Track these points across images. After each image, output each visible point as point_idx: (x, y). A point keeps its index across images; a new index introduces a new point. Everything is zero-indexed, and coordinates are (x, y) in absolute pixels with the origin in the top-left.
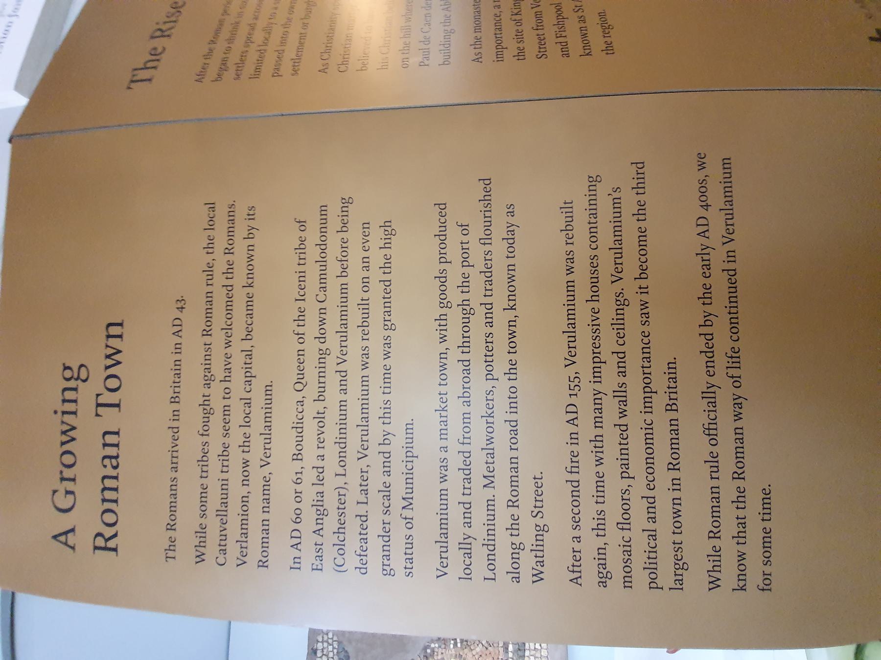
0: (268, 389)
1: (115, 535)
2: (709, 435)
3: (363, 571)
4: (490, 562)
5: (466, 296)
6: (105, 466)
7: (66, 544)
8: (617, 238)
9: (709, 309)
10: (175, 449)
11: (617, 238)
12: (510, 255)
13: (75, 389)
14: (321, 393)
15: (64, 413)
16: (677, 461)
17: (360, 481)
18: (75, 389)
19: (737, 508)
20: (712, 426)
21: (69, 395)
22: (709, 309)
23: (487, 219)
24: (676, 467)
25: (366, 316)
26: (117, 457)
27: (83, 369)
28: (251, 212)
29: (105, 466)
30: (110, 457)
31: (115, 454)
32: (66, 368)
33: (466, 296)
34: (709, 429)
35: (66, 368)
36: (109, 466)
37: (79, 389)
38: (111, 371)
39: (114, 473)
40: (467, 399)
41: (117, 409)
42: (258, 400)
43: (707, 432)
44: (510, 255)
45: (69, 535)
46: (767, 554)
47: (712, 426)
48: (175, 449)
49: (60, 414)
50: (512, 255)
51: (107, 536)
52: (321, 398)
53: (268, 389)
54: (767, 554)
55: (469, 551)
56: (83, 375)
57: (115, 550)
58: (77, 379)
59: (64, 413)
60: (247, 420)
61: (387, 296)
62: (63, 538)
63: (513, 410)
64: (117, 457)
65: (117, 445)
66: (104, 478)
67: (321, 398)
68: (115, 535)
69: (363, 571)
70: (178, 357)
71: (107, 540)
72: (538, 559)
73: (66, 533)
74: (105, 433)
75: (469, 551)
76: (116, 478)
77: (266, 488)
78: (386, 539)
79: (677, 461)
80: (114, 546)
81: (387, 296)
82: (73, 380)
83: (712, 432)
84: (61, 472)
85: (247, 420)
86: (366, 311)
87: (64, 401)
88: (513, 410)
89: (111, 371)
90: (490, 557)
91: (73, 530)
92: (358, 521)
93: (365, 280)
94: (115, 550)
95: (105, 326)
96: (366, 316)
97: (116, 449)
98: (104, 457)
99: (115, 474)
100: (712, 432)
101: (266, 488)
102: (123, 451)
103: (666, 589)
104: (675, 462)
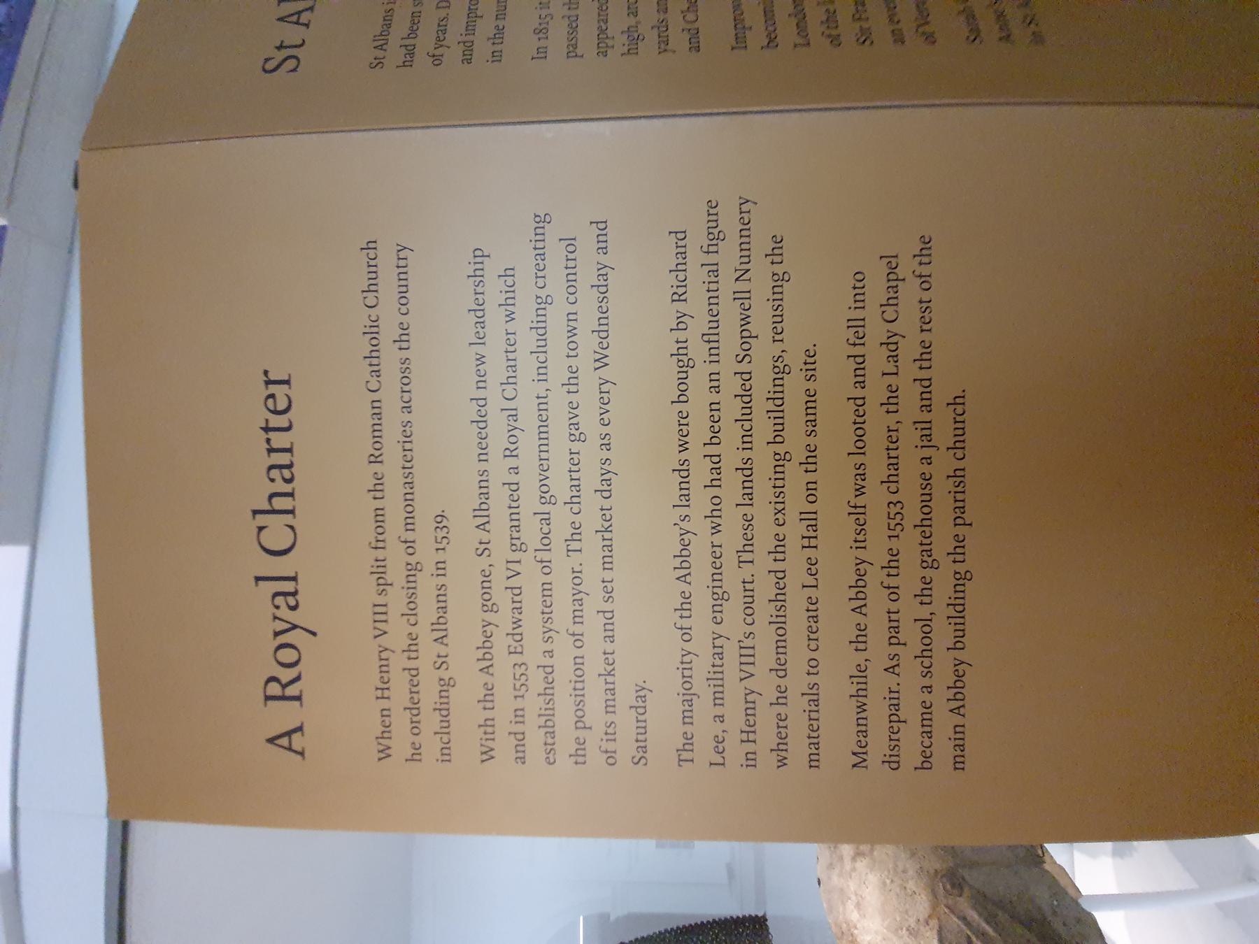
1: (298, 678)
3: (606, 494)
6: (272, 480)
7: (290, 749)
19: (921, 368)
25: (780, 427)
26: (290, 466)
28: (860, 538)
29: (272, 480)
30: (281, 467)
31: (292, 590)
38: (283, 639)
39: (287, 488)
41: (297, 703)
51: (284, 681)
57: (298, 698)
60: (546, 541)
61: (859, 420)
62: (284, 741)
64: (290, 466)
68: (298, 678)
69: (606, 494)
70: (441, 580)
71: (284, 686)
73: (289, 734)
76: (291, 495)
80: (296, 693)
81: (859, 420)
84: (268, 441)
85: (546, 541)
86: (780, 421)
89: (283, 639)
91: (300, 729)
94: (298, 698)
95: (265, 471)
96: (780, 427)
97: (293, 583)
98: (271, 467)
99: (290, 491)
103: (943, 449)
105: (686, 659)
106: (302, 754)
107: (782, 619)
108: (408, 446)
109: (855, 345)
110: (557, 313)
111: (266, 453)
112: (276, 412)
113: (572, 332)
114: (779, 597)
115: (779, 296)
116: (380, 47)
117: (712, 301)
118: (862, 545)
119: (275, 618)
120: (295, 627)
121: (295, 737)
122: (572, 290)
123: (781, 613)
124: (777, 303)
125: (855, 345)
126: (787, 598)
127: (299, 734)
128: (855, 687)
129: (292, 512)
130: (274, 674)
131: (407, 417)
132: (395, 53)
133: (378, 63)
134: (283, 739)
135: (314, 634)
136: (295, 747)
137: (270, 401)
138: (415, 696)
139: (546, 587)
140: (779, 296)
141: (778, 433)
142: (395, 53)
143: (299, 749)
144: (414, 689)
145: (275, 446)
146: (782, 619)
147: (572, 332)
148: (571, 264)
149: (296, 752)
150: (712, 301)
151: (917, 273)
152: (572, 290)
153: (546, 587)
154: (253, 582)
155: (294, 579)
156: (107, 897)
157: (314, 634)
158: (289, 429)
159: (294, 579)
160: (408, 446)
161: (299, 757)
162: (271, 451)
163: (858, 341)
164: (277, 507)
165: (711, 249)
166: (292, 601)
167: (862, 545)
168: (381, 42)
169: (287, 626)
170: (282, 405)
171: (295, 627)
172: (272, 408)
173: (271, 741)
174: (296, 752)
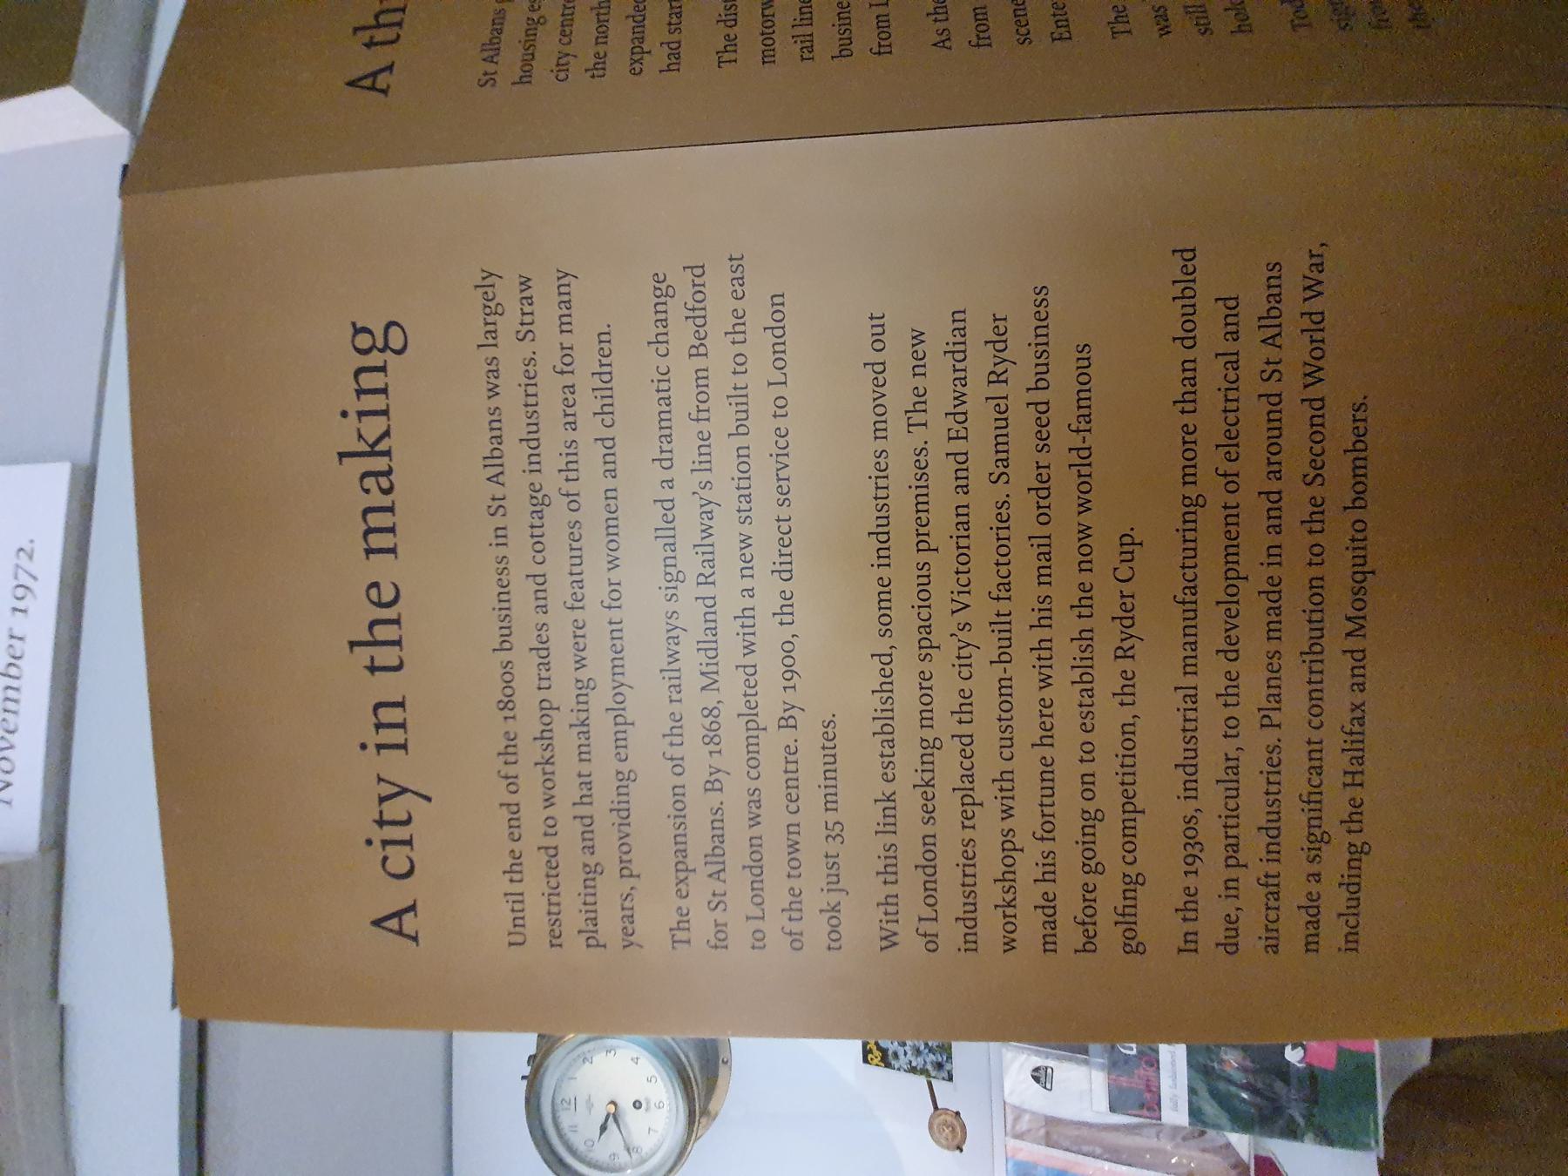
0: (604, 337)
5: (892, 890)
6: (367, 491)
7: (400, 933)
8: (957, 325)
11: (957, 325)
13: (383, 369)
15: (361, 414)
18: (383, 369)
26: (389, 473)
27: (394, 329)
29: (367, 491)
32: (358, 331)
33: (892, 890)
35: (358, 331)
36: (374, 489)
37: (389, 368)
39: (386, 501)
40: (889, 737)
42: (587, 360)
46: (885, 620)
49: (353, 416)
53: (604, 337)
54: (885, 620)
55: (671, 541)
56: (396, 343)
62: (393, 924)
63: (882, 561)
64: (389, 473)
66: (366, 512)
73: (398, 914)
74: (378, 706)
75: (671, 541)
76: (391, 509)
77: (611, 523)
82: (375, 352)
87: (360, 392)
88: (882, 561)
90: (778, 348)
91: (412, 908)
93: (776, 300)
95: (371, 709)
97: (386, 459)
98: (365, 475)
101: (611, 523)
102: (395, 401)
106: (415, 939)
107: (889, 714)
108: (531, 390)
110: (733, 409)
111: (363, 555)
112: (380, 605)
113: (794, 847)
114: (885, 687)
115: (1044, 340)
116: (490, 60)
120: (404, 790)
121: (408, 917)
123: (887, 706)
124: (1041, 348)
126: (895, 687)
129: (398, 643)
131: (542, 618)
132: (511, 57)
133: (489, 80)
134: (392, 921)
135: (429, 799)
136: (406, 930)
137: (374, 592)
139: (700, 374)
140: (1044, 340)
141: (1041, 376)
142: (511, 57)
146: (889, 714)
147: (794, 847)
148: (791, 767)
153: (700, 374)
154: (347, 647)
155: (401, 705)
156: (182, 1139)
157: (429, 799)
159: (401, 705)
160: (531, 390)
164: (380, 638)
166: (385, 483)
168: (492, 50)
169: (396, 789)
170: (388, 596)
171: (404, 790)
172: (375, 598)
173: (377, 923)
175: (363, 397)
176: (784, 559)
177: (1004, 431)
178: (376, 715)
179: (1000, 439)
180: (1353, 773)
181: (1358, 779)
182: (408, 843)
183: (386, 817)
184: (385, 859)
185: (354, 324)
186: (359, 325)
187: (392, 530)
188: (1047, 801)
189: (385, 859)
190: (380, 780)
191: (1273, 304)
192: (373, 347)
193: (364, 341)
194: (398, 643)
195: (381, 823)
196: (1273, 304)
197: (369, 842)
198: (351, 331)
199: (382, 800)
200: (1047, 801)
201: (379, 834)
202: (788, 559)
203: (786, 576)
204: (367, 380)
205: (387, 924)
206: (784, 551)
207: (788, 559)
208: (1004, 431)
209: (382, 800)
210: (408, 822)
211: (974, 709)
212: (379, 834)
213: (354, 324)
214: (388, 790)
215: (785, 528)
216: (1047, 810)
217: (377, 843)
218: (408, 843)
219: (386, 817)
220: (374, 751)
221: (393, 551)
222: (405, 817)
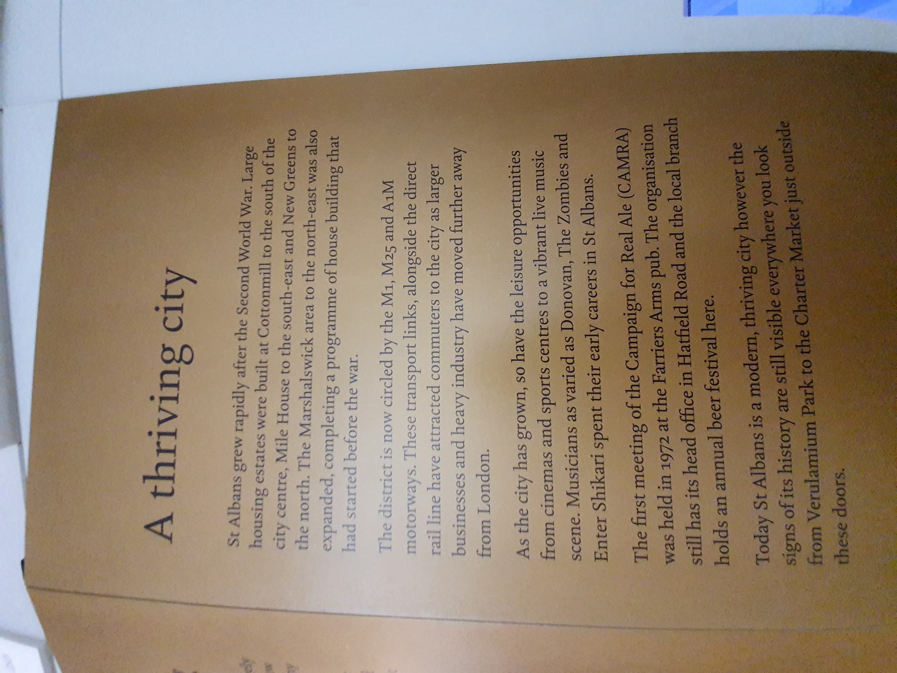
2: (686, 421)
4: (485, 534)
7: (161, 534)
9: (389, 336)
10: (167, 427)
11: (541, 239)
12: (309, 296)
13: (177, 373)
14: (263, 383)
15: (162, 399)
16: (631, 253)
17: (256, 447)
18: (177, 373)
20: (688, 412)
21: (169, 379)
22: (389, 336)
23: (457, 219)
24: (630, 258)
27: (186, 350)
32: (165, 349)
34: (685, 415)
41: (173, 437)
43: (683, 417)
44: (309, 296)
45: (165, 524)
47: (688, 412)
48: (167, 427)
49: (155, 435)
50: (311, 296)
52: (263, 388)
58: (178, 362)
59: (162, 399)
62: (158, 528)
65: (177, 385)
67: (263, 388)
72: (434, 443)
73: (162, 522)
78: (329, 501)
79: (631, 253)
83: (688, 418)
84: (158, 443)
87: (163, 385)
91: (170, 518)
92: (323, 486)
99: (180, 305)
100: (688, 418)
104: (682, 291)
105: (435, 234)
106: (170, 538)
109: (627, 286)
117: (543, 343)
118: (696, 494)
119: (160, 409)
120: (181, 277)
122: (436, 369)
125: (627, 286)
127: (169, 522)
128: (595, 491)
129: (172, 478)
130: (163, 370)
135: (195, 282)
136: (165, 533)
138: (263, 410)
143: (169, 535)
144: (262, 405)
145: (163, 447)
149: (166, 537)
150: (543, 343)
151: (782, 504)
152: (436, 369)
157: (195, 282)
158: (172, 494)
161: (168, 541)
162: (160, 451)
163: (629, 284)
164: (161, 474)
165: (641, 521)
167: (696, 494)
169: (177, 276)
171: (181, 277)
173: (148, 527)
174: (166, 537)
175: (161, 454)
176: (412, 186)
177: (542, 178)
178: (162, 378)
179: (539, 182)
180: (684, 356)
181: (687, 360)
182: (181, 309)
183: (158, 491)
184: (166, 319)
185: (163, 345)
186: (166, 346)
187: (173, 465)
188: (516, 199)
189: (166, 319)
190: (168, 271)
191: (760, 459)
192: (173, 359)
193: (168, 355)
194: (172, 478)
195: (165, 297)
196: (760, 459)
197: (152, 398)
198: (162, 349)
199: (168, 283)
200: (516, 199)
201: (163, 304)
202: (414, 186)
203: (412, 196)
204: (168, 379)
205: (153, 528)
206: (412, 182)
207: (414, 186)
208: (542, 178)
209: (168, 283)
210: (181, 296)
211: (529, 522)
212: (163, 304)
213: (163, 345)
214: (171, 277)
215: (412, 169)
216: (516, 204)
217: (157, 399)
218: (181, 309)
219: (158, 491)
220: (163, 310)
221: (176, 399)
222: (179, 293)
